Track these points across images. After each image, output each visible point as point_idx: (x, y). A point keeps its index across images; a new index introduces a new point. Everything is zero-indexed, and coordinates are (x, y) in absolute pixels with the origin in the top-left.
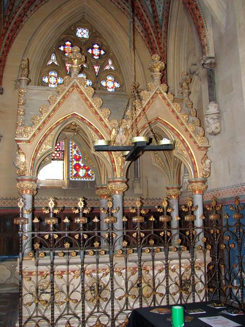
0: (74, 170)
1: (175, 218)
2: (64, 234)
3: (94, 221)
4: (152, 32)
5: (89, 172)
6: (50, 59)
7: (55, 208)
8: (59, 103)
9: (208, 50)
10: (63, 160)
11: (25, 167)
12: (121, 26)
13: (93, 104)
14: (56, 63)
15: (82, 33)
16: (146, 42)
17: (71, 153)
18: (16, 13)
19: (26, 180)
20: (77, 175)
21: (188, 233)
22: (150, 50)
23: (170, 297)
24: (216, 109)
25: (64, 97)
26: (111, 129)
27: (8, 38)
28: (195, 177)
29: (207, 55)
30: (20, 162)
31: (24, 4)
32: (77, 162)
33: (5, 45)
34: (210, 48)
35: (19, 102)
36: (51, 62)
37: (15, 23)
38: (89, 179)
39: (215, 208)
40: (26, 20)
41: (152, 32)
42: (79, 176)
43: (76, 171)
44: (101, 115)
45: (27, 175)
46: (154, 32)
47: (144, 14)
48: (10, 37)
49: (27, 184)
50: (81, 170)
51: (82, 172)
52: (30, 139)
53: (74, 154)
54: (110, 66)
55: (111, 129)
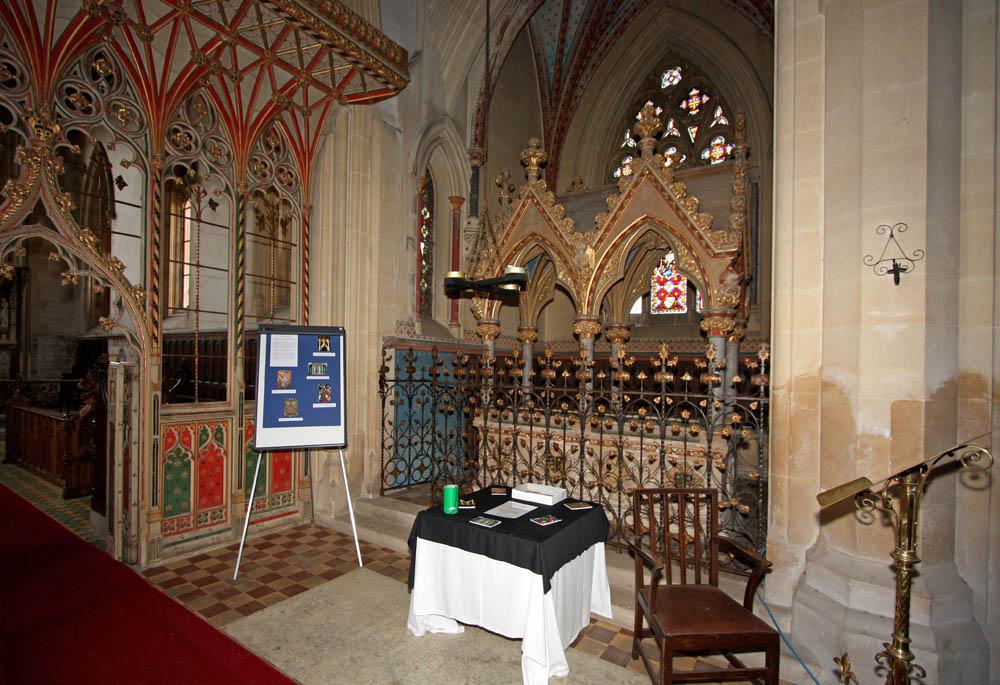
1: (528, 372)
2: (683, 398)
3: (684, 378)
7: (670, 358)
12: (729, 39)
20: (662, 307)
21: (543, 395)
23: (585, 491)
36: (714, 123)
39: (666, 361)
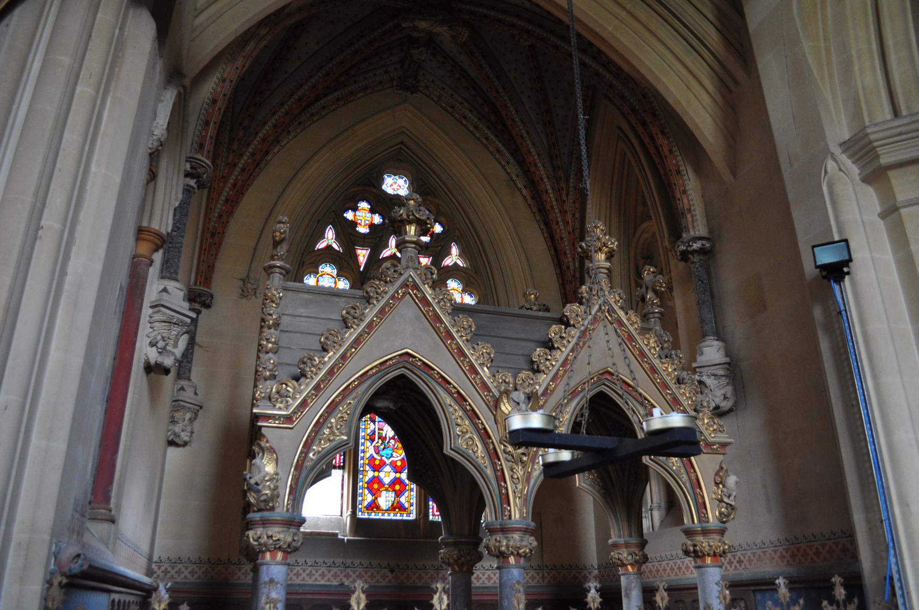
0: (366, 491)
4: (549, 187)
5: (403, 499)
6: (322, 236)
8: (370, 326)
9: (693, 222)
10: (343, 468)
11: (276, 488)
13: (453, 331)
14: (335, 246)
15: (395, 187)
16: (535, 210)
17: (363, 451)
18: (257, 133)
19: (274, 523)
20: (373, 506)
22: (543, 226)
24: (722, 352)
25: (382, 312)
26: (497, 394)
27: (234, 185)
28: (700, 521)
29: (692, 233)
30: (262, 474)
31: (276, 117)
32: (376, 474)
33: (227, 201)
34: (698, 217)
35: (263, 320)
37: (253, 154)
38: (402, 515)
40: (276, 151)
41: (549, 187)
42: (378, 508)
43: (373, 495)
44: (473, 359)
45: (278, 510)
46: (553, 189)
47: (532, 150)
48: (239, 183)
49: (278, 533)
50: (384, 493)
51: (386, 499)
52: (294, 412)
53: (368, 455)
54: (454, 258)
55: (497, 394)
